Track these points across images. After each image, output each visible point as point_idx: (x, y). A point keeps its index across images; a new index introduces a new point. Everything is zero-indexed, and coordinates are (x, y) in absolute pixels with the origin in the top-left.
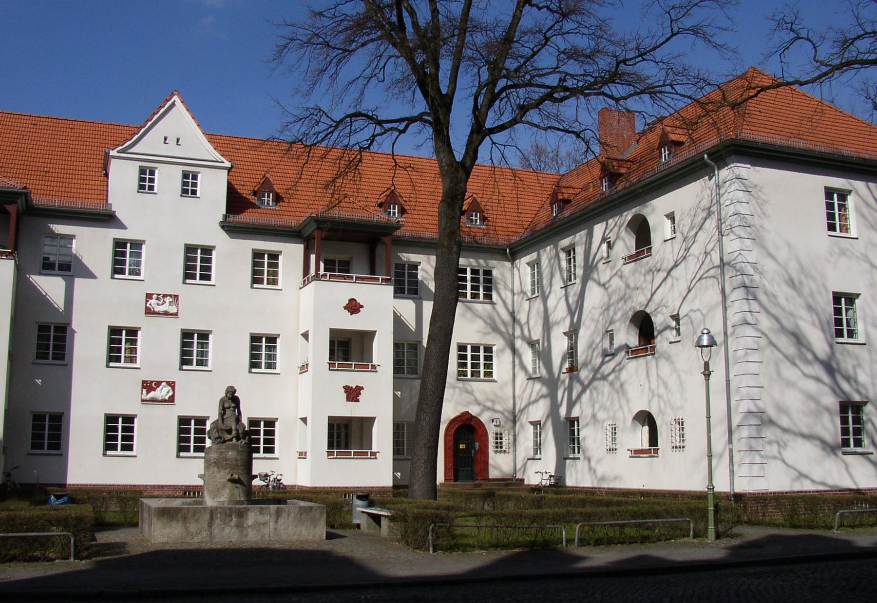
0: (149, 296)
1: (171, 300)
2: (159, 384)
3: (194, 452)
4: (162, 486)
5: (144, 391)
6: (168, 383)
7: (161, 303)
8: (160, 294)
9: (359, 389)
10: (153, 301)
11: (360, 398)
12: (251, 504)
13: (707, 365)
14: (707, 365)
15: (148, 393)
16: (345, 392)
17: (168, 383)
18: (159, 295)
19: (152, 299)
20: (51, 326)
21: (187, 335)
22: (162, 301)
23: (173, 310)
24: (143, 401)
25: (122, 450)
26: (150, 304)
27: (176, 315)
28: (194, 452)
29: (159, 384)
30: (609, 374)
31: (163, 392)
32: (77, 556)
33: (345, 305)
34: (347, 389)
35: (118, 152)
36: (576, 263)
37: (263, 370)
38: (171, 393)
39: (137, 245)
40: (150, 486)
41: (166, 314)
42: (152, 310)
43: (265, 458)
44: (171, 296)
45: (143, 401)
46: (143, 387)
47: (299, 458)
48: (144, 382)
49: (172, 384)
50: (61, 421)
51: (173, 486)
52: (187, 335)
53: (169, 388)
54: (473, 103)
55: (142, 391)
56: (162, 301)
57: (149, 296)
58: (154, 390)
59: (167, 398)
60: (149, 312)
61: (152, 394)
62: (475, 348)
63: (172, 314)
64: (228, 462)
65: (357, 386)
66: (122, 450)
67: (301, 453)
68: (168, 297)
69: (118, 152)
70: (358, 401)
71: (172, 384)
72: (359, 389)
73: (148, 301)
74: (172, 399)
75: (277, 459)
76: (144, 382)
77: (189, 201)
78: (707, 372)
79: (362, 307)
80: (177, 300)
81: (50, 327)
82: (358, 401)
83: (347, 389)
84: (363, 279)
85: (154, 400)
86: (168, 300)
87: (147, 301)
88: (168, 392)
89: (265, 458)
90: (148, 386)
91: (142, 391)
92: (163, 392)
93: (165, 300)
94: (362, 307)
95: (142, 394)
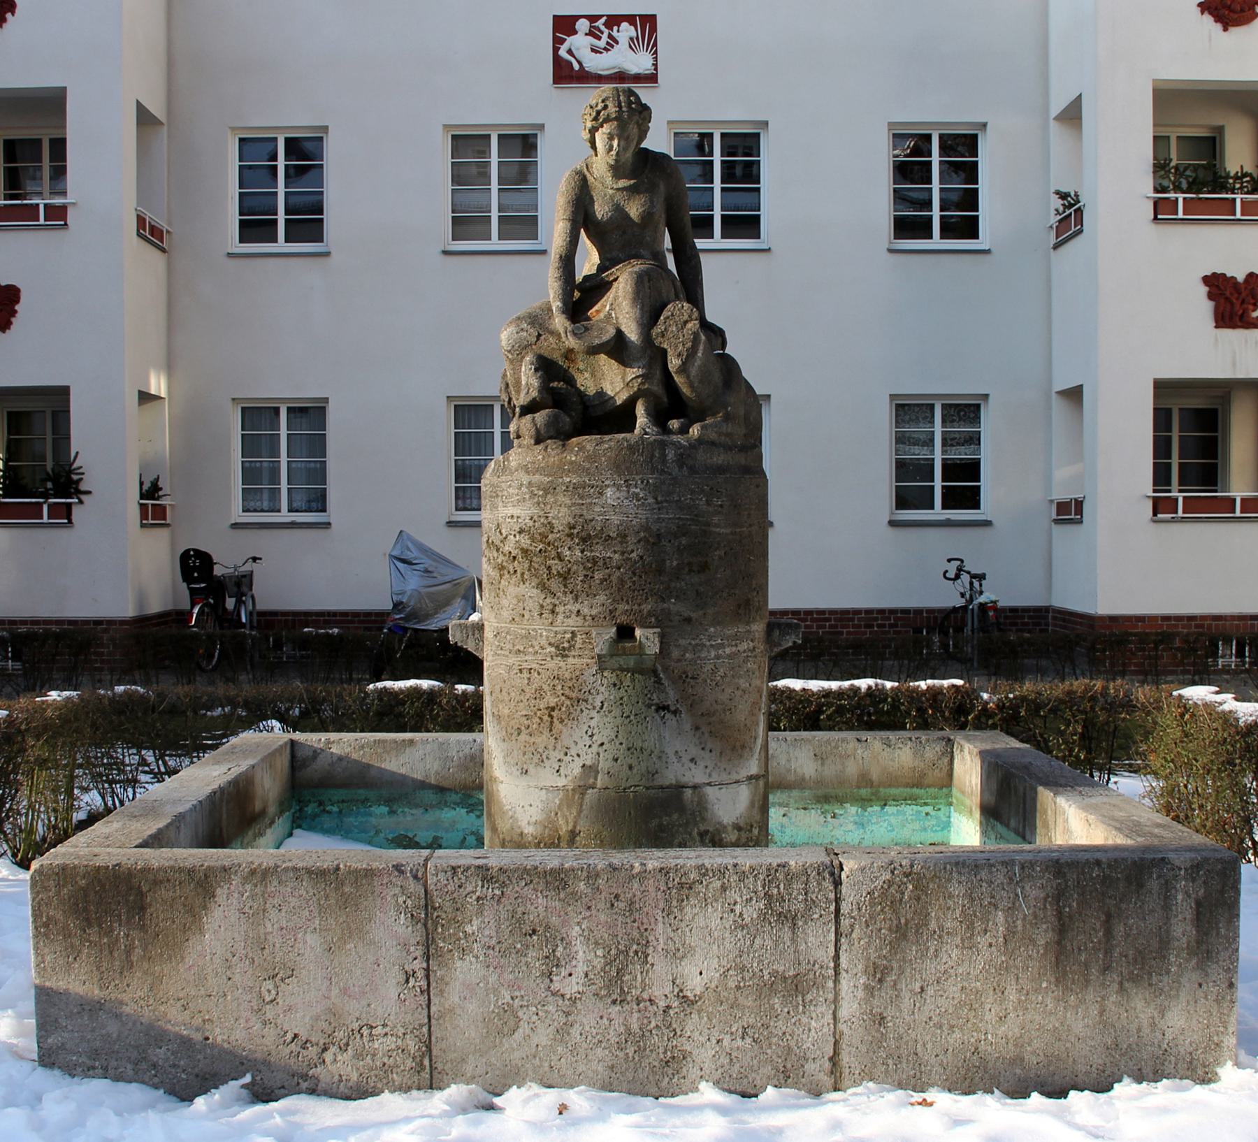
0: (564, 25)
3: (944, 507)
7: (602, 43)
8: (600, 17)
10: (579, 43)
12: (828, 680)
16: (1211, 296)
18: (593, 19)
19: (575, 32)
22: (605, 37)
25: (945, 506)
26: (570, 52)
28: (944, 507)
30: (106, 804)
37: (936, 241)
42: (576, 66)
43: (948, 524)
44: (630, 19)
47: (1057, 521)
56: (605, 37)
57: (564, 25)
64: (600, 552)
66: (945, 506)
67: (1063, 507)
68: (624, 25)
73: (562, 41)
75: (987, 523)
80: (653, 29)
81: (931, 407)
86: (626, 32)
87: (557, 42)
89: (948, 524)
93: (615, 33)
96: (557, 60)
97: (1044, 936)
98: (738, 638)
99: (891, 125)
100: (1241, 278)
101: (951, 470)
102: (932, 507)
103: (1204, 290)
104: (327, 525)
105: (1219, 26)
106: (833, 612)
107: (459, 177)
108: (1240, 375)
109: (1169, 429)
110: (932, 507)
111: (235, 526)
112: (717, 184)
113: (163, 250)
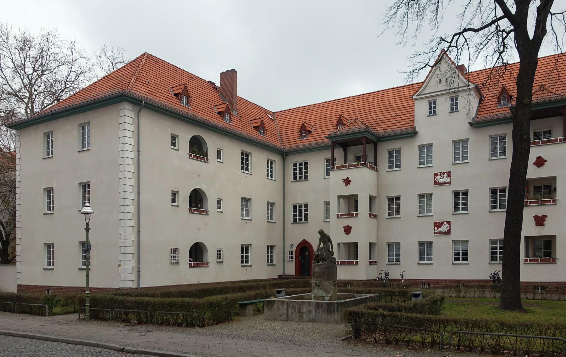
0: (436, 175)
1: (447, 175)
2: (442, 223)
4: (445, 280)
5: (436, 228)
6: (447, 222)
7: (442, 177)
9: (544, 217)
10: (438, 177)
11: (545, 223)
13: (87, 224)
14: (87, 224)
15: (437, 229)
16: (535, 220)
17: (447, 222)
18: (441, 173)
20: (302, 205)
21: (456, 194)
23: (448, 180)
24: (435, 233)
26: (437, 179)
27: (450, 183)
29: (442, 223)
31: (444, 228)
32: (397, 316)
33: (534, 162)
34: (536, 218)
35: (417, 96)
36: (54, 194)
38: (448, 228)
39: (430, 146)
40: (440, 280)
41: (445, 183)
43: (396, 264)
44: (446, 172)
45: (435, 233)
46: (435, 226)
48: (435, 223)
49: (449, 223)
50: (551, 244)
51: (451, 280)
52: (456, 194)
53: (447, 225)
54: (504, 19)
55: (435, 228)
57: (436, 175)
58: (440, 227)
59: (446, 231)
60: (436, 183)
61: (440, 229)
62: (300, 206)
63: (447, 183)
65: (543, 215)
69: (417, 96)
70: (543, 225)
71: (449, 223)
72: (544, 217)
74: (449, 232)
76: (435, 223)
77: (85, 180)
78: (87, 229)
79: (546, 161)
80: (450, 174)
82: (543, 225)
83: (536, 218)
84: (352, 166)
85: (440, 233)
86: (446, 175)
87: (435, 178)
88: (447, 228)
90: (438, 225)
91: (435, 228)
92: (444, 228)
94: (546, 161)
95: (435, 229)
96: (435, 181)
97: (244, 317)
98: (328, 283)
99: (490, 188)
100: (541, 216)
101: (463, 254)
102: (497, 260)
103: (533, 219)
104: (432, 264)
105: (537, 167)
106: (479, 280)
107: (455, 199)
108: (540, 235)
109: (50, 260)
110: (497, 260)
111: (387, 264)
112: (498, 199)
113: (376, 218)
